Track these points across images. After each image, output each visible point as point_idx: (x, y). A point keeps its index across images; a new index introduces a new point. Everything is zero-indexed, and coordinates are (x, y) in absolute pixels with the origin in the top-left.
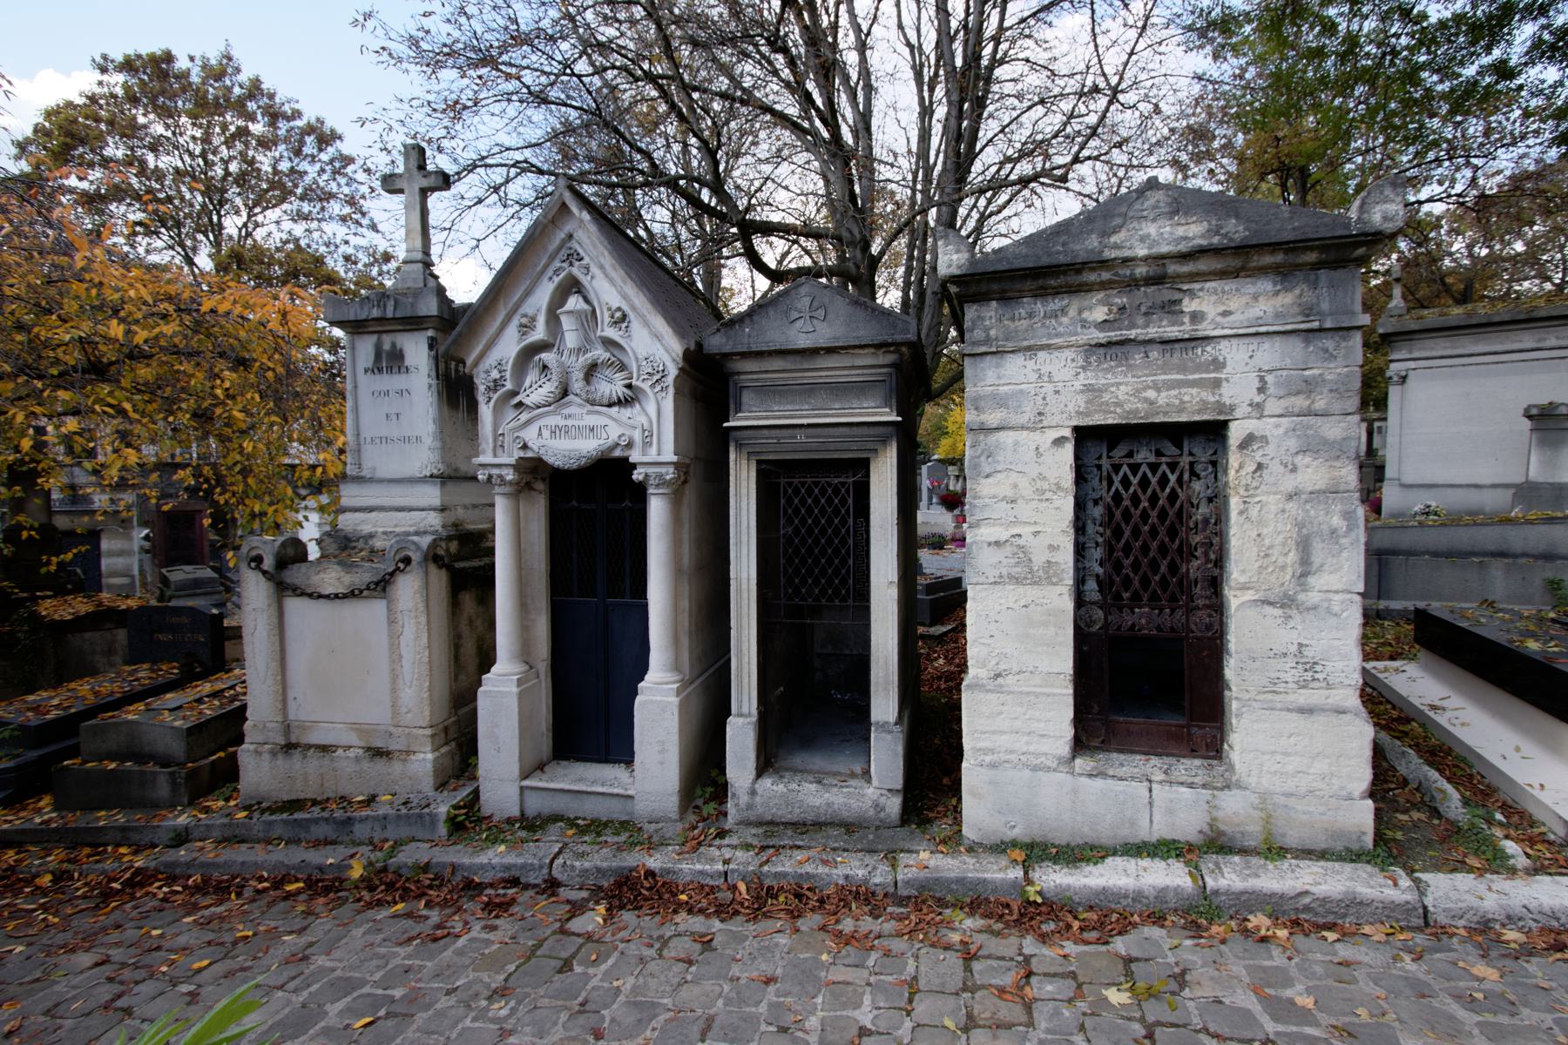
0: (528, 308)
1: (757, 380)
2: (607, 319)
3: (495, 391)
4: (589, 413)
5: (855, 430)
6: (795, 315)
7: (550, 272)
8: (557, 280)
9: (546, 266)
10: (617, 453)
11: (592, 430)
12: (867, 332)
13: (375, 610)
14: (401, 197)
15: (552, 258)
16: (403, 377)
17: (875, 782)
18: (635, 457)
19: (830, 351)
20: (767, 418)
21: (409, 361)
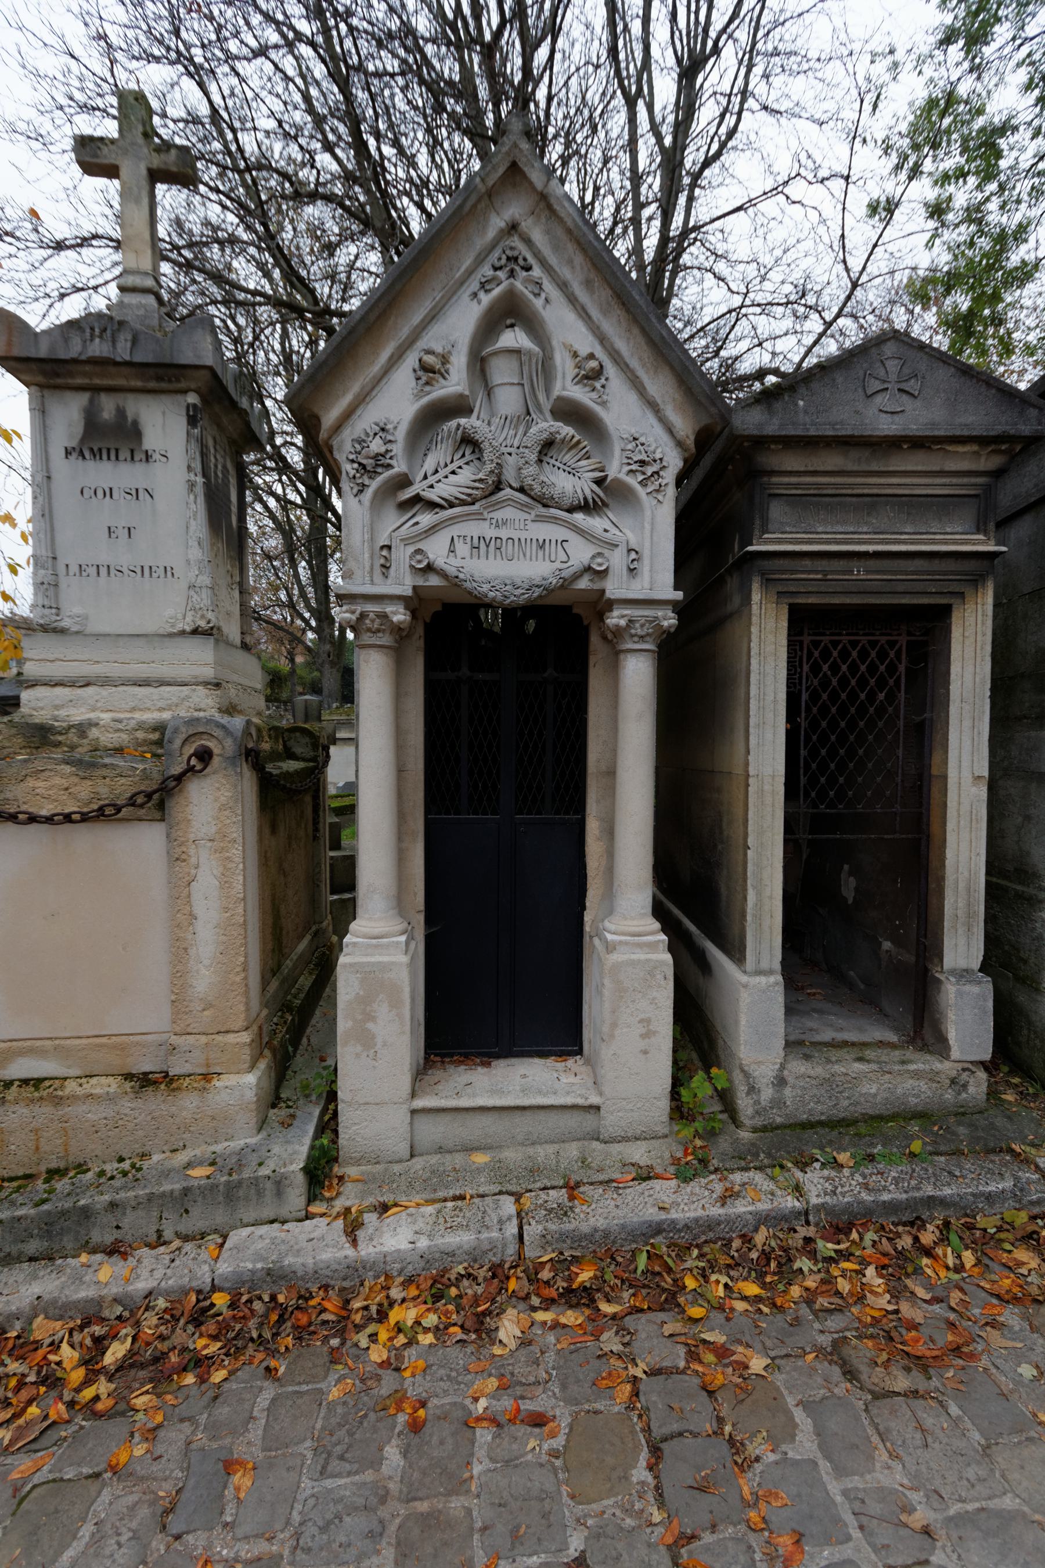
0: (434, 339)
1: (797, 486)
2: (571, 371)
3: (373, 474)
4: (539, 519)
5: (936, 565)
6: (875, 385)
7: (474, 285)
8: (486, 299)
9: (470, 272)
10: (583, 584)
11: (542, 546)
12: (977, 417)
13: (142, 843)
14: (113, 186)
15: (479, 261)
16: (139, 468)
17: (955, 1054)
18: (614, 588)
19: (918, 443)
20: (810, 542)
21: (151, 440)
